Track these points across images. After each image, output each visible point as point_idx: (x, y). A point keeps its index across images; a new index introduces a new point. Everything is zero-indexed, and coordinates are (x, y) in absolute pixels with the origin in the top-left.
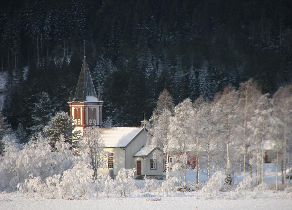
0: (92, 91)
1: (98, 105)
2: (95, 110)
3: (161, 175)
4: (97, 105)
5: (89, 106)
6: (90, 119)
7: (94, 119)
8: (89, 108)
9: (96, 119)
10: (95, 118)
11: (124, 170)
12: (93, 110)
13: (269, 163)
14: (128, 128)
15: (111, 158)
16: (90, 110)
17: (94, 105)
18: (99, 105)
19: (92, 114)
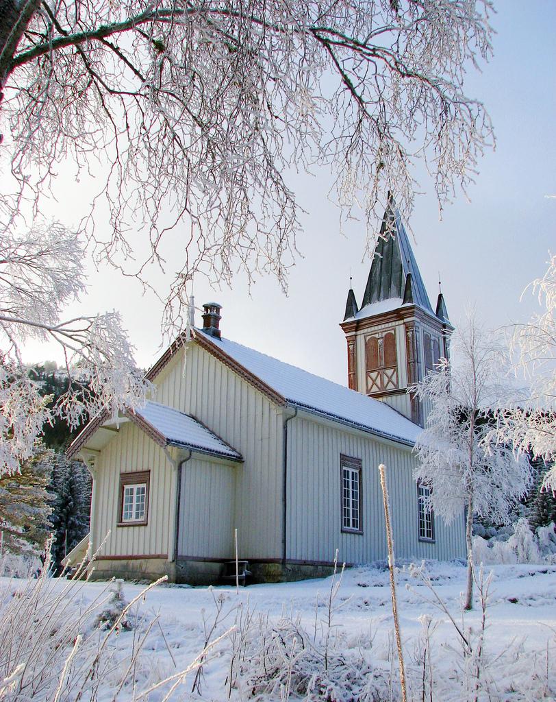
0: (392, 285)
1: (402, 322)
2: (390, 340)
3: (166, 557)
4: (397, 323)
5: (366, 331)
6: (374, 375)
7: (390, 372)
8: (368, 338)
9: (396, 370)
10: (391, 368)
11: (281, 412)
12: (380, 341)
13: (130, 630)
14: (320, 582)
15: (135, 496)
16: (371, 346)
17: (387, 325)
18: (406, 320)
19: (381, 352)
